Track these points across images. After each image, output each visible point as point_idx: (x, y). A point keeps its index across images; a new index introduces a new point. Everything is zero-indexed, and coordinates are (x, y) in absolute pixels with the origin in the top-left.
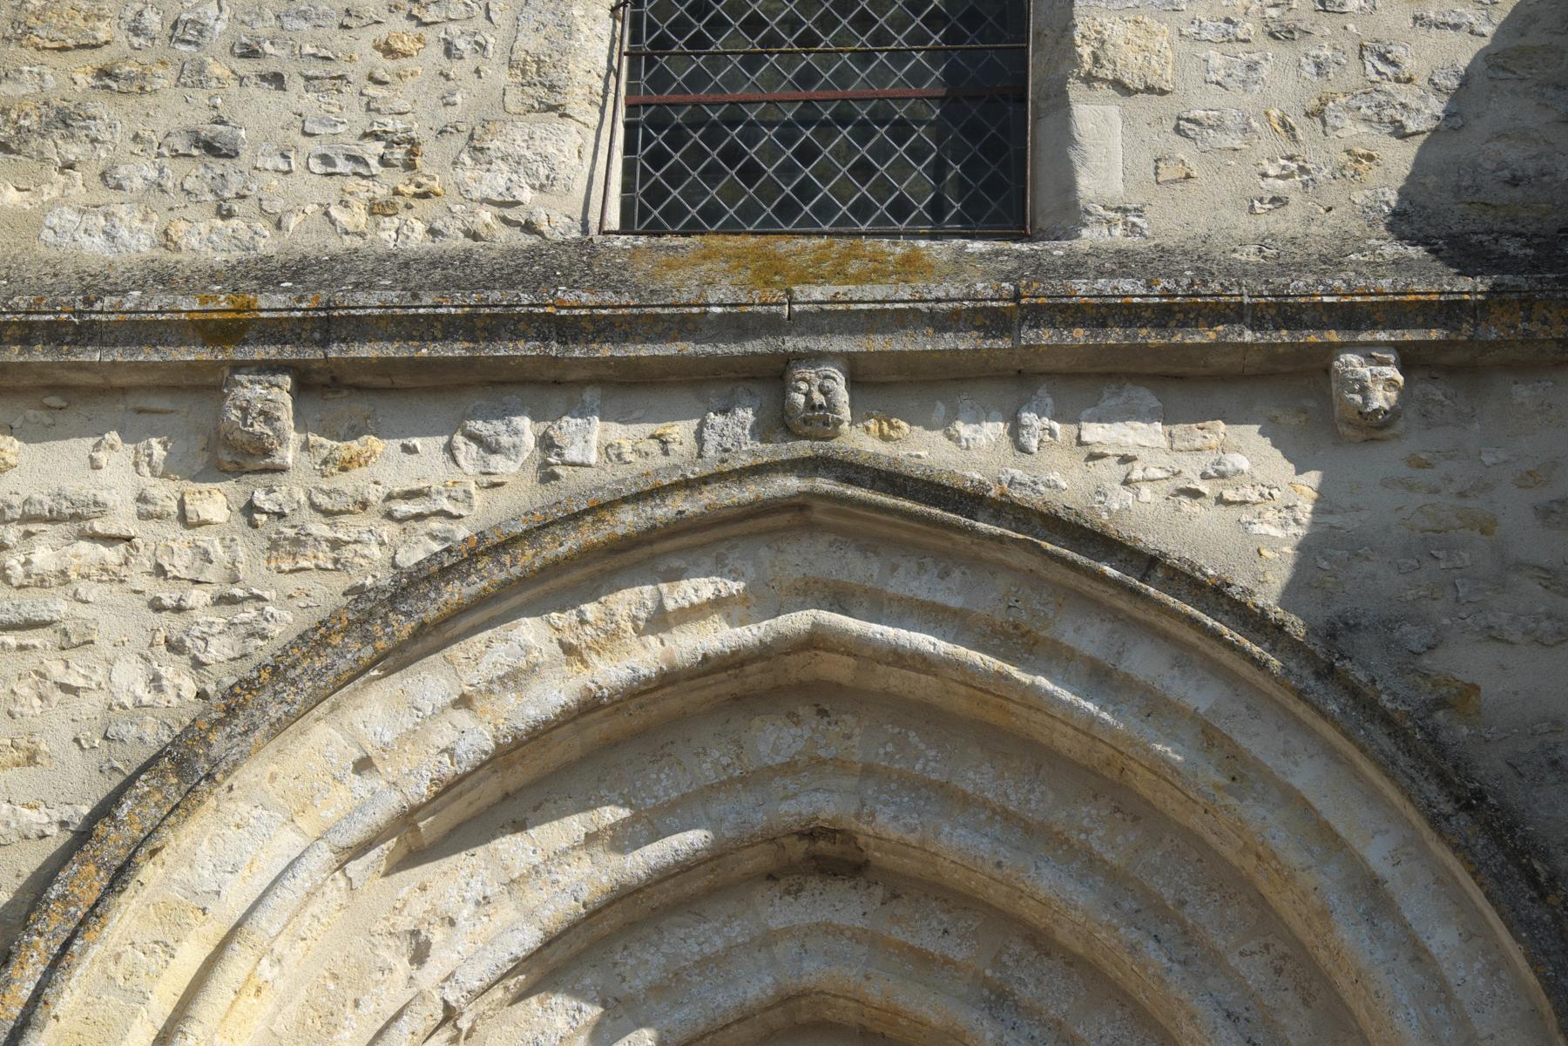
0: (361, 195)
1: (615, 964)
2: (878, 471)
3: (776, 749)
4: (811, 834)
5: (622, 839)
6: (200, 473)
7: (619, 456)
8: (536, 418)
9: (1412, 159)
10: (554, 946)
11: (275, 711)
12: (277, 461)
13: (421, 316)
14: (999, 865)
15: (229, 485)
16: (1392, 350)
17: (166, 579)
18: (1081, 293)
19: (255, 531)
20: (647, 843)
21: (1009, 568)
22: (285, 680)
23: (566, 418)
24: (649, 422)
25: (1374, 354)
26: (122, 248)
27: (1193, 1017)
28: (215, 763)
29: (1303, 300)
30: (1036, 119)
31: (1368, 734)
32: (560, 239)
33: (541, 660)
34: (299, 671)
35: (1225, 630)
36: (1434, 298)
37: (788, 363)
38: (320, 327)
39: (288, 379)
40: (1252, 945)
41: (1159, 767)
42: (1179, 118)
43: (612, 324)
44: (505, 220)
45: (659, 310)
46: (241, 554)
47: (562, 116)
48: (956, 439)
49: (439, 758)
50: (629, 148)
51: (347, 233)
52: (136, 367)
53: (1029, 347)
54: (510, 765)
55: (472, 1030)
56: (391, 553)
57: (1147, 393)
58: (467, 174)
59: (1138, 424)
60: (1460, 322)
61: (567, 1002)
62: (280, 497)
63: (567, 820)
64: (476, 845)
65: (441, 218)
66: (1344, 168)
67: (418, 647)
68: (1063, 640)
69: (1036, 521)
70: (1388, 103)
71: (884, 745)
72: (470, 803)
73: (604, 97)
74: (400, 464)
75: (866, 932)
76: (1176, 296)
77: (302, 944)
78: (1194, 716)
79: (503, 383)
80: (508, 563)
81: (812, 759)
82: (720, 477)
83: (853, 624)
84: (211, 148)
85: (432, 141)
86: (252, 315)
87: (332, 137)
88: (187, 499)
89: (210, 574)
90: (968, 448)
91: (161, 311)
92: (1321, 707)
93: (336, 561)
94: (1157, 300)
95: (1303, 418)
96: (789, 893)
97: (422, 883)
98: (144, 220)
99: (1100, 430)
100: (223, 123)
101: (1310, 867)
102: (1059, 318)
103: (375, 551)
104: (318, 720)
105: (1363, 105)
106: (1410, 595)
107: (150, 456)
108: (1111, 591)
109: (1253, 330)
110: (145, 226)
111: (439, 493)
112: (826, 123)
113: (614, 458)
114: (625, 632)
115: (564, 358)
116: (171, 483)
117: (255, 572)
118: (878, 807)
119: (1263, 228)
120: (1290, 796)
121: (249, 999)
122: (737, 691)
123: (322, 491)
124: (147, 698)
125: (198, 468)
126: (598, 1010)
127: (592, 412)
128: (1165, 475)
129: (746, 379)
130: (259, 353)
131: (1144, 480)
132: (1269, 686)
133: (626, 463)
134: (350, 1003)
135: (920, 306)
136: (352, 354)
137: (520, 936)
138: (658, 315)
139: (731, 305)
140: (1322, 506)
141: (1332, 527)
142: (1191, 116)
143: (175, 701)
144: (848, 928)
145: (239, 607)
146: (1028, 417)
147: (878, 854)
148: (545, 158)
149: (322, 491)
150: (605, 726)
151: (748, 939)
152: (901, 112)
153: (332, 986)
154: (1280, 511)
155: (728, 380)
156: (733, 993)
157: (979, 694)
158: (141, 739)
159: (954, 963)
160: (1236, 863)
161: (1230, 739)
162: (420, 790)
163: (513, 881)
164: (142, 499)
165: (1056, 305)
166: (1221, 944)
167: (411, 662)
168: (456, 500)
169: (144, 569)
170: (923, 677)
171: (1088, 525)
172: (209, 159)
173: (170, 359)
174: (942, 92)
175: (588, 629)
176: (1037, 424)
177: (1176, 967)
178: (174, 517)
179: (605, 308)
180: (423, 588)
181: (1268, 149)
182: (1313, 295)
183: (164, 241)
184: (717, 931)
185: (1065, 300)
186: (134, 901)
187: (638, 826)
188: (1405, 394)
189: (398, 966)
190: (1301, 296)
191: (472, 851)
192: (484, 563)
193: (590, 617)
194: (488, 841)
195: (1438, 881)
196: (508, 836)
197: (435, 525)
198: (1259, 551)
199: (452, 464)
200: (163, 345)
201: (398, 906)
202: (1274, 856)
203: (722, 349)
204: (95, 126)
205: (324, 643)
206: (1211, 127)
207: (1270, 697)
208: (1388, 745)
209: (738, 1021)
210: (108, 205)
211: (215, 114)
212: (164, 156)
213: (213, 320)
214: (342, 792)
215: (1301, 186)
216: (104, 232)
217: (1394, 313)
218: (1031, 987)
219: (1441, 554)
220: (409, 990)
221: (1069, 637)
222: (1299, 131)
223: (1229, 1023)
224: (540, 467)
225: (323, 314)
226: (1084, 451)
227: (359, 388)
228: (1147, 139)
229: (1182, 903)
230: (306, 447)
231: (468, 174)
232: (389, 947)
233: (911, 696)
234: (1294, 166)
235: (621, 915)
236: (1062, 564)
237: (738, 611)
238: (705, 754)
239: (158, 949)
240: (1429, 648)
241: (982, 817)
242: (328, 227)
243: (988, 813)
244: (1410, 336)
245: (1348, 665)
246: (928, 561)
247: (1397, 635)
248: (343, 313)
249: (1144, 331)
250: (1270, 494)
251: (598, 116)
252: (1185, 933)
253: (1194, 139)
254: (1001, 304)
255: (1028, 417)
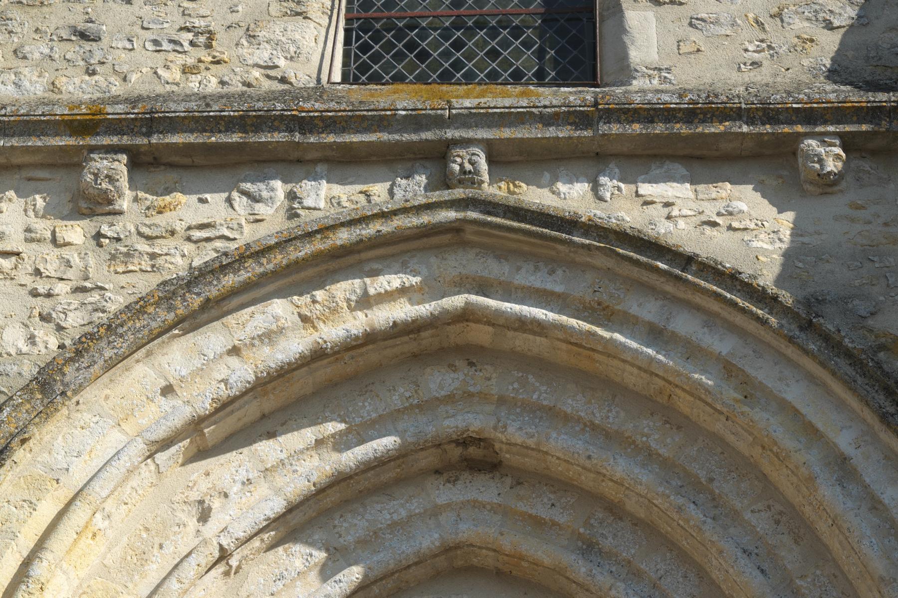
0: (178, 63)
1: (335, 527)
2: (508, 207)
3: (441, 387)
4: (464, 442)
5: (341, 443)
6: (66, 216)
7: (339, 204)
8: (285, 181)
9: (838, 41)
10: (294, 513)
11: (108, 353)
12: (117, 207)
13: (211, 117)
14: (589, 457)
15: (85, 223)
16: (838, 137)
17: (41, 277)
18: (637, 102)
19: (100, 249)
20: (355, 447)
21: (594, 268)
22: (116, 334)
23: (304, 181)
24: (359, 184)
25: (826, 139)
26: (24, 92)
27: (721, 552)
28: (67, 385)
29: (780, 106)
30: (602, 21)
31: (836, 364)
32: (303, 86)
33: (286, 325)
34: (125, 328)
35: (739, 300)
36: (864, 105)
37: (448, 147)
38: (146, 124)
39: (125, 157)
40: (759, 506)
41: (695, 391)
42: (691, 18)
43: (335, 122)
44: (268, 77)
45: (365, 113)
46: (91, 262)
47: (305, 18)
48: (557, 193)
49: (218, 385)
50: (347, 42)
51: (168, 83)
52: (27, 150)
53: (604, 135)
54: (265, 394)
55: (239, 568)
56: (189, 261)
57: (680, 166)
58: (246, 50)
59: (675, 184)
60: (880, 119)
61: (302, 550)
62: (118, 228)
63: (303, 431)
64: (243, 447)
65: (228, 75)
66: (796, 46)
67: (205, 316)
68: (631, 311)
69: (612, 237)
70: (821, 10)
71: (512, 384)
72: (239, 419)
73: (332, 10)
74: (196, 209)
75: (500, 505)
76: (699, 103)
77: (125, 507)
78: (719, 358)
79: (264, 161)
80: (265, 263)
81: (465, 393)
82: (404, 211)
83: (492, 303)
84: (84, 36)
85: (223, 32)
86: (102, 117)
87: (160, 31)
88: (57, 230)
89: (70, 274)
90: (565, 199)
91: (43, 115)
92: (805, 347)
93: (153, 266)
94: (686, 106)
95: (780, 181)
96: (449, 482)
97: (207, 471)
98: (39, 77)
99: (650, 188)
100: (92, 22)
101: (800, 450)
102: (623, 118)
103: (179, 260)
104: (138, 361)
105: (806, 11)
106: (857, 283)
107: (35, 205)
108: (662, 279)
109: (748, 125)
110: (41, 79)
111: (221, 225)
112: (470, 28)
113: (335, 205)
114: (342, 308)
115: (303, 143)
116: (48, 221)
117: (98, 271)
118: (509, 422)
119: (747, 79)
120: (785, 408)
121: (86, 541)
122: (415, 350)
123: (145, 225)
124: (25, 349)
125: (65, 213)
126: (323, 555)
127: (322, 178)
128: (692, 213)
129: (421, 158)
130: (106, 141)
131: (680, 216)
132: (768, 337)
133: (343, 207)
134: (156, 546)
135: (533, 110)
136: (167, 141)
137: (271, 504)
138: (364, 116)
139: (412, 110)
140: (797, 232)
141: (803, 243)
142: (699, 16)
143: (43, 351)
144: (489, 503)
145: (88, 294)
146: (603, 180)
147: (508, 456)
148: (294, 41)
149: (145, 225)
150: (328, 370)
151: (422, 511)
152: (516, 22)
153: (145, 535)
154: (769, 234)
155: (409, 160)
156: (413, 544)
157: (575, 348)
158: (20, 374)
159: (559, 525)
160: (747, 454)
161: (743, 371)
162: (205, 406)
163: (267, 469)
164: (28, 230)
165: (621, 109)
166: (738, 505)
167: (200, 326)
168: (233, 229)
169: (28, 272)
170: (538, 338)
171: (646, 238)
172: (82, 42)
173: (48, 144)
174: (542, 10)
175: (318, 306)
176: (609, 184)
177: (709, 520)
178: (48, 241)
179: (330, 111)
180: (209, 278)
181: (749, 37)
182: (786, 103)
183: (52, 88)
184: (402, 505)
185: (627, 106)
186: (10, 474)
187: (350, 436)
188: (846, 163)
189: (190, 524)
190: (778, 104)
191: (240, 451)
192: (250, 263)
193: (319, 298)
194: (251, 444)
195: (886, 457)
196: (264, 441)
197: (219, 244)
198: (757, 257)
199: (230, 209)
200: (44, 136)
201: (190, 484)
202: (776, 443)
203: (406, 137)
204: (12, 24)
205: (142, 311)
206: (712, 23)
207: (769, 345)
208: (850, 371)
209: (416, 564)
210: (18, 67)
211: (87, 17)
212: (54, 40)
213: (77, 120)
214: (153, 407)
215: (769, 56)
216: (14, 83)
217: (838, 114)
218: (610, 539)
219: (875, 259)
220: (197, 539)
221: (634, 310)
222: (766, 26)
223: (745, 556)
224: (287, 210)
225: (148, 116)
226: (641, 200)
227: (172, 166)
228: (672, 30)
229: (712, 480)
230: (136, 199)
231: (245, 50)
232: (183, 511)
233: (529, 354)
234: (764, 45)
235: (338, 494)
236: (630, 262)
237: (416, 296)
238: (394, 390)
239: (25, 505)
240: (872, 314)
241: (577, 429)
242: (156, 80)
243: (581, 426)
244: (848, 128)
245: (822, 321)
246: (541, 264)
247: (850, 306)
248: (161, 115)
249: (678, 126)
250: (762, 224)
251: (328, 21)
252: (714, 499)
253: (701, 30)
254: (586, 109)
255: (603, 180)
